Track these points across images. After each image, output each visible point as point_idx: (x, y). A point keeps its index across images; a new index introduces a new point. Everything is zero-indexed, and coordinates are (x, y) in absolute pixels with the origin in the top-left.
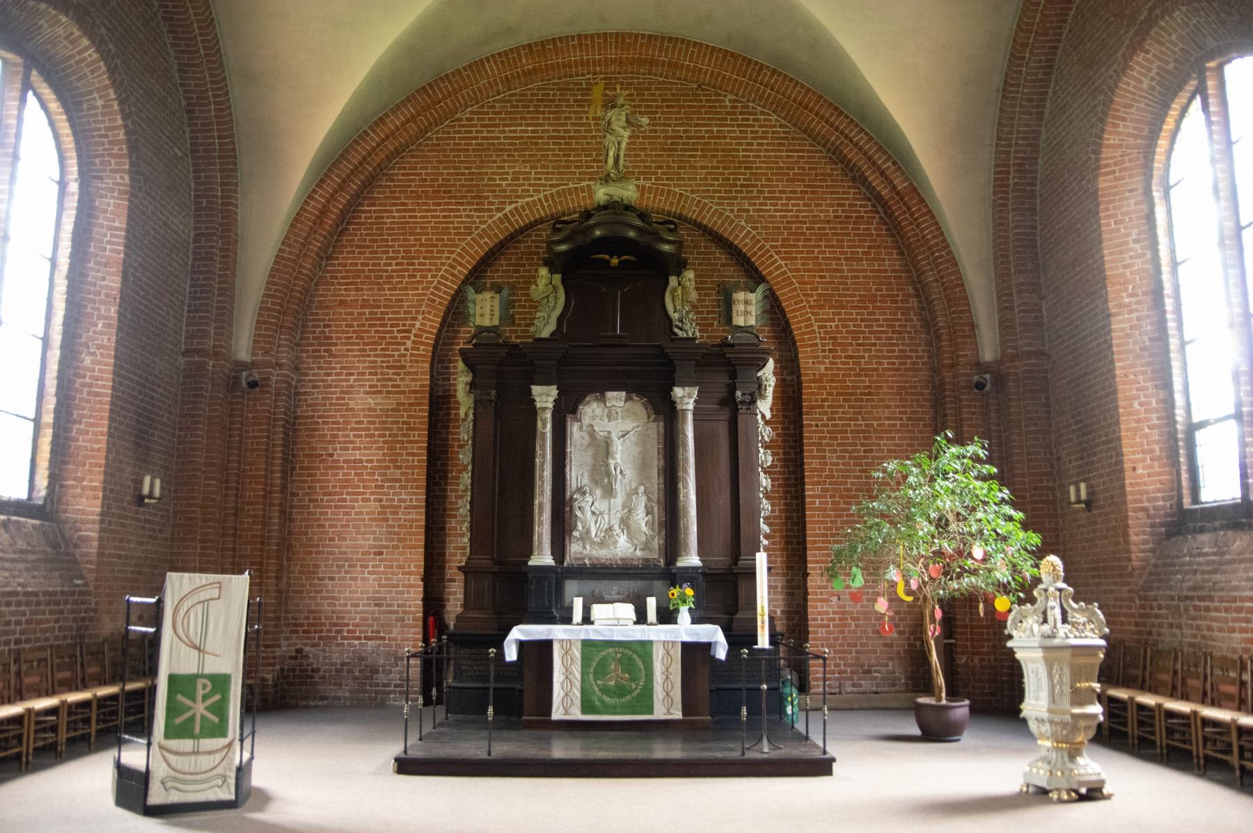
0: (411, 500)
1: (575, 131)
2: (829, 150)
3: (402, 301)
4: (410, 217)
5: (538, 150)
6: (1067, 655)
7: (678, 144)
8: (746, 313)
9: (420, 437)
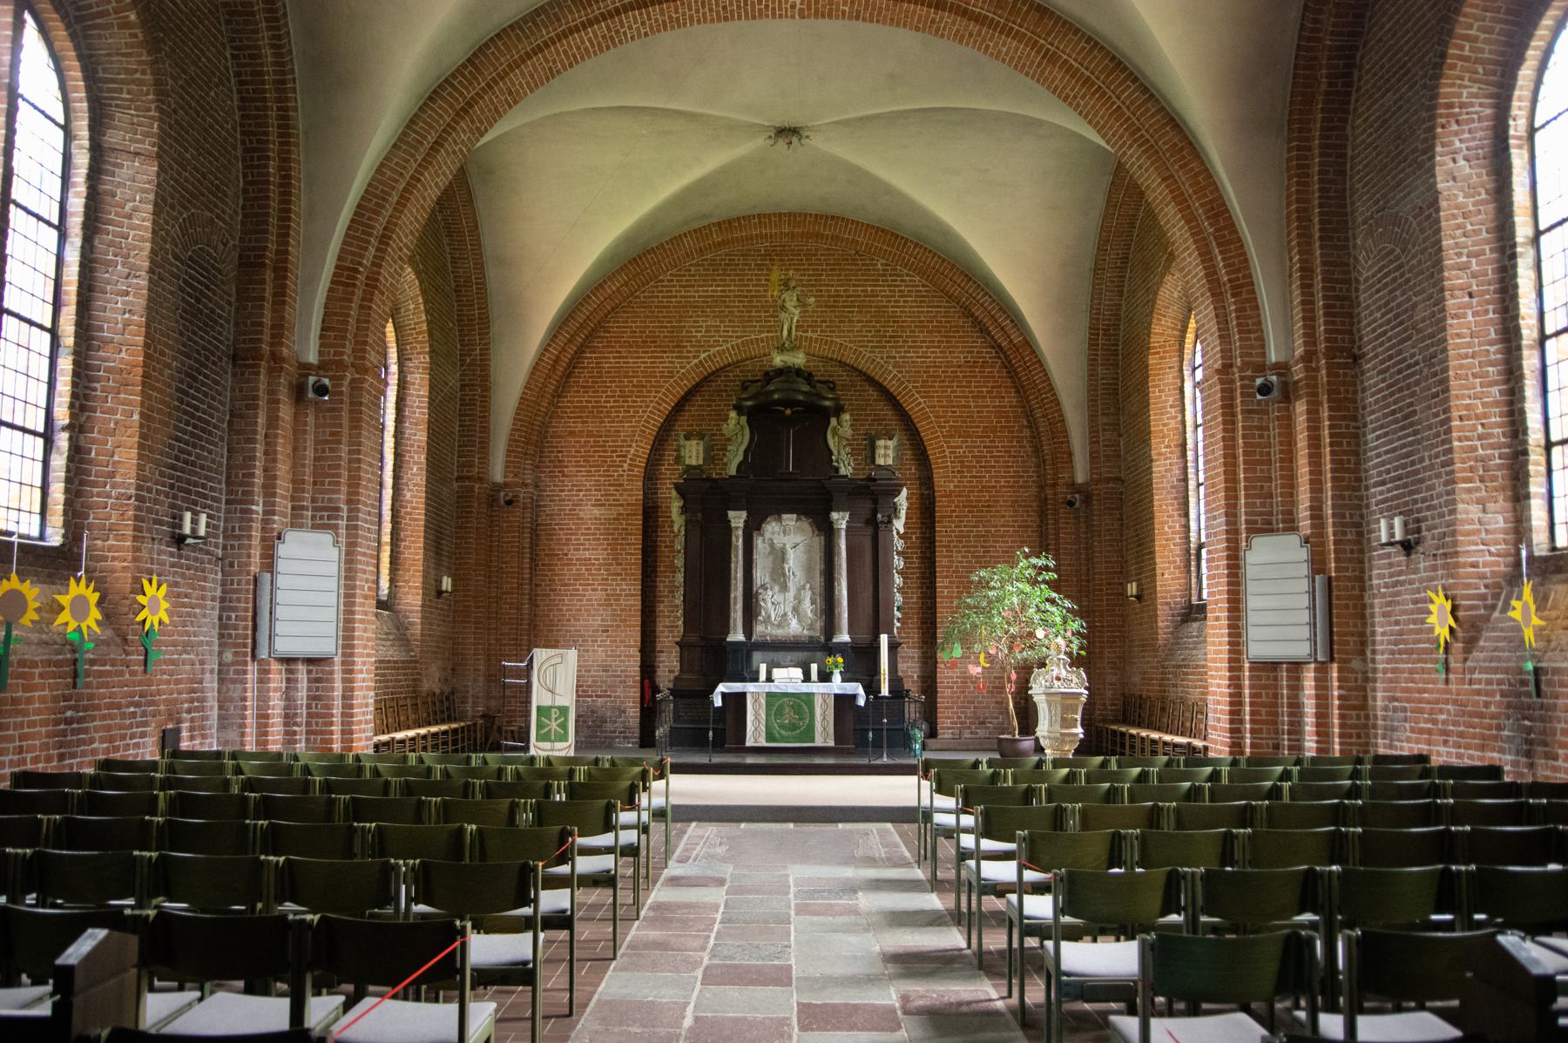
0: (630, 591)
6: (1058, 698)
8: (886, 456)
9: (636, 540)
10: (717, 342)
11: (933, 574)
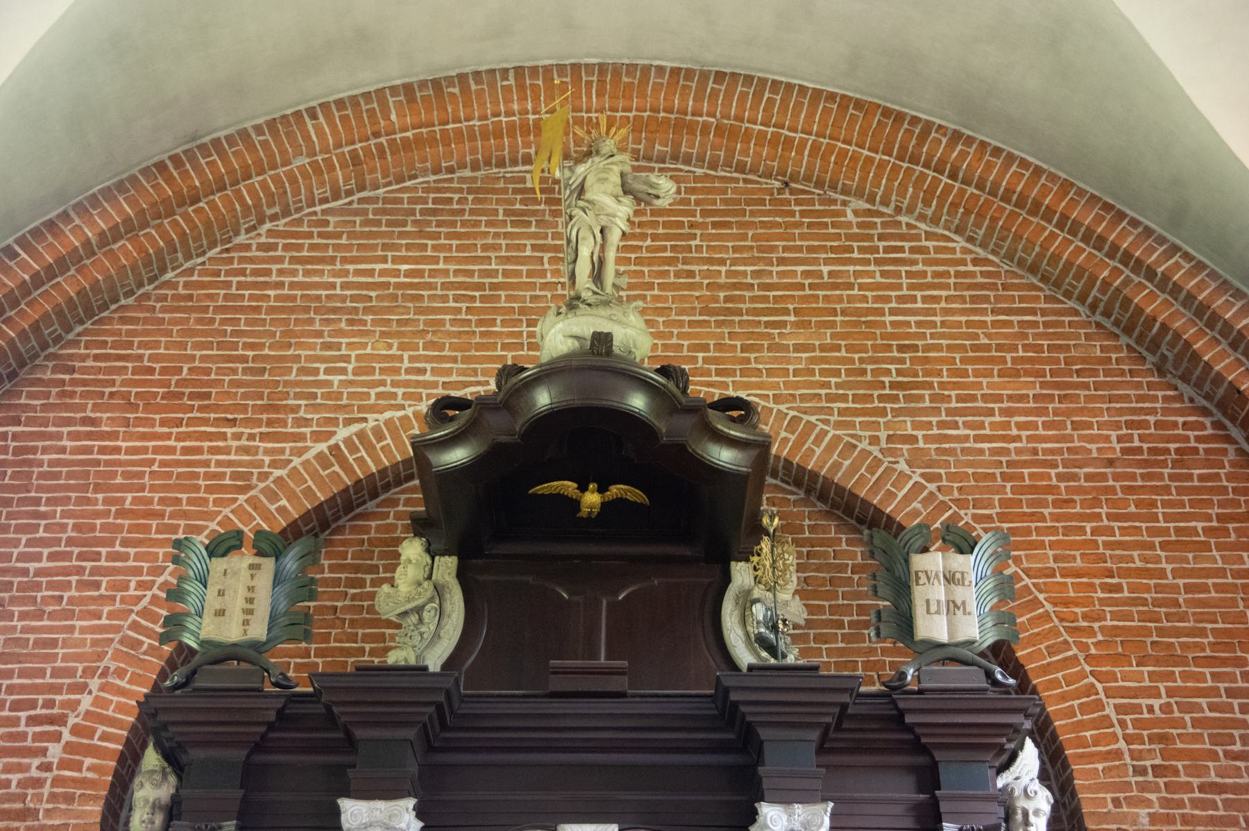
1: (506, 273)
2: (1093, 308)
3: (53, 643)
4: (102, 450)
5: (419, 311)
7: (741, 299)
8: (953, 606)
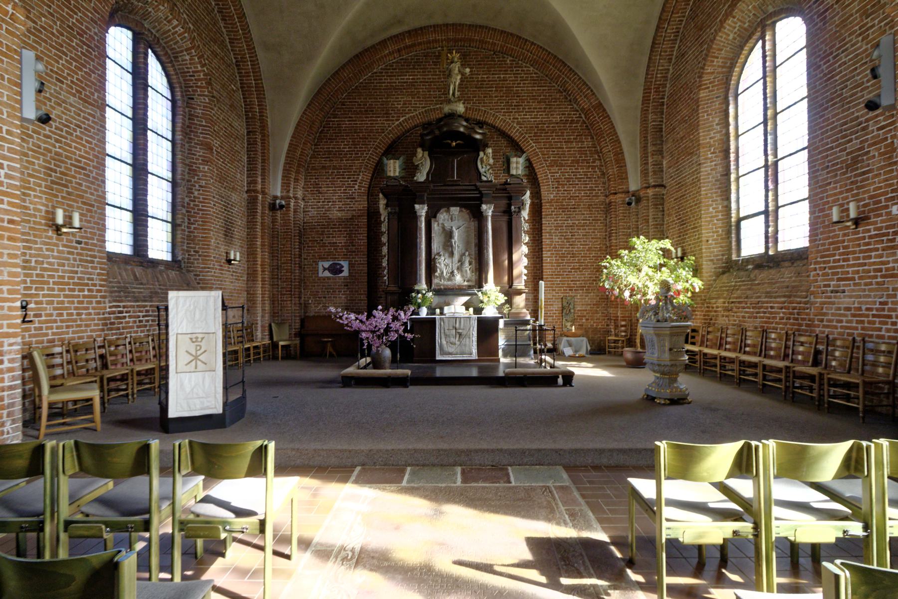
10: (410, 112)
11: (541, 250)
